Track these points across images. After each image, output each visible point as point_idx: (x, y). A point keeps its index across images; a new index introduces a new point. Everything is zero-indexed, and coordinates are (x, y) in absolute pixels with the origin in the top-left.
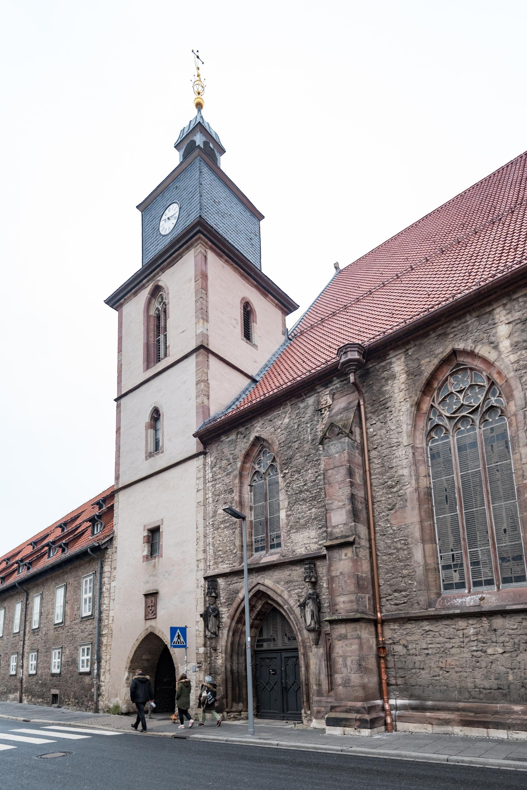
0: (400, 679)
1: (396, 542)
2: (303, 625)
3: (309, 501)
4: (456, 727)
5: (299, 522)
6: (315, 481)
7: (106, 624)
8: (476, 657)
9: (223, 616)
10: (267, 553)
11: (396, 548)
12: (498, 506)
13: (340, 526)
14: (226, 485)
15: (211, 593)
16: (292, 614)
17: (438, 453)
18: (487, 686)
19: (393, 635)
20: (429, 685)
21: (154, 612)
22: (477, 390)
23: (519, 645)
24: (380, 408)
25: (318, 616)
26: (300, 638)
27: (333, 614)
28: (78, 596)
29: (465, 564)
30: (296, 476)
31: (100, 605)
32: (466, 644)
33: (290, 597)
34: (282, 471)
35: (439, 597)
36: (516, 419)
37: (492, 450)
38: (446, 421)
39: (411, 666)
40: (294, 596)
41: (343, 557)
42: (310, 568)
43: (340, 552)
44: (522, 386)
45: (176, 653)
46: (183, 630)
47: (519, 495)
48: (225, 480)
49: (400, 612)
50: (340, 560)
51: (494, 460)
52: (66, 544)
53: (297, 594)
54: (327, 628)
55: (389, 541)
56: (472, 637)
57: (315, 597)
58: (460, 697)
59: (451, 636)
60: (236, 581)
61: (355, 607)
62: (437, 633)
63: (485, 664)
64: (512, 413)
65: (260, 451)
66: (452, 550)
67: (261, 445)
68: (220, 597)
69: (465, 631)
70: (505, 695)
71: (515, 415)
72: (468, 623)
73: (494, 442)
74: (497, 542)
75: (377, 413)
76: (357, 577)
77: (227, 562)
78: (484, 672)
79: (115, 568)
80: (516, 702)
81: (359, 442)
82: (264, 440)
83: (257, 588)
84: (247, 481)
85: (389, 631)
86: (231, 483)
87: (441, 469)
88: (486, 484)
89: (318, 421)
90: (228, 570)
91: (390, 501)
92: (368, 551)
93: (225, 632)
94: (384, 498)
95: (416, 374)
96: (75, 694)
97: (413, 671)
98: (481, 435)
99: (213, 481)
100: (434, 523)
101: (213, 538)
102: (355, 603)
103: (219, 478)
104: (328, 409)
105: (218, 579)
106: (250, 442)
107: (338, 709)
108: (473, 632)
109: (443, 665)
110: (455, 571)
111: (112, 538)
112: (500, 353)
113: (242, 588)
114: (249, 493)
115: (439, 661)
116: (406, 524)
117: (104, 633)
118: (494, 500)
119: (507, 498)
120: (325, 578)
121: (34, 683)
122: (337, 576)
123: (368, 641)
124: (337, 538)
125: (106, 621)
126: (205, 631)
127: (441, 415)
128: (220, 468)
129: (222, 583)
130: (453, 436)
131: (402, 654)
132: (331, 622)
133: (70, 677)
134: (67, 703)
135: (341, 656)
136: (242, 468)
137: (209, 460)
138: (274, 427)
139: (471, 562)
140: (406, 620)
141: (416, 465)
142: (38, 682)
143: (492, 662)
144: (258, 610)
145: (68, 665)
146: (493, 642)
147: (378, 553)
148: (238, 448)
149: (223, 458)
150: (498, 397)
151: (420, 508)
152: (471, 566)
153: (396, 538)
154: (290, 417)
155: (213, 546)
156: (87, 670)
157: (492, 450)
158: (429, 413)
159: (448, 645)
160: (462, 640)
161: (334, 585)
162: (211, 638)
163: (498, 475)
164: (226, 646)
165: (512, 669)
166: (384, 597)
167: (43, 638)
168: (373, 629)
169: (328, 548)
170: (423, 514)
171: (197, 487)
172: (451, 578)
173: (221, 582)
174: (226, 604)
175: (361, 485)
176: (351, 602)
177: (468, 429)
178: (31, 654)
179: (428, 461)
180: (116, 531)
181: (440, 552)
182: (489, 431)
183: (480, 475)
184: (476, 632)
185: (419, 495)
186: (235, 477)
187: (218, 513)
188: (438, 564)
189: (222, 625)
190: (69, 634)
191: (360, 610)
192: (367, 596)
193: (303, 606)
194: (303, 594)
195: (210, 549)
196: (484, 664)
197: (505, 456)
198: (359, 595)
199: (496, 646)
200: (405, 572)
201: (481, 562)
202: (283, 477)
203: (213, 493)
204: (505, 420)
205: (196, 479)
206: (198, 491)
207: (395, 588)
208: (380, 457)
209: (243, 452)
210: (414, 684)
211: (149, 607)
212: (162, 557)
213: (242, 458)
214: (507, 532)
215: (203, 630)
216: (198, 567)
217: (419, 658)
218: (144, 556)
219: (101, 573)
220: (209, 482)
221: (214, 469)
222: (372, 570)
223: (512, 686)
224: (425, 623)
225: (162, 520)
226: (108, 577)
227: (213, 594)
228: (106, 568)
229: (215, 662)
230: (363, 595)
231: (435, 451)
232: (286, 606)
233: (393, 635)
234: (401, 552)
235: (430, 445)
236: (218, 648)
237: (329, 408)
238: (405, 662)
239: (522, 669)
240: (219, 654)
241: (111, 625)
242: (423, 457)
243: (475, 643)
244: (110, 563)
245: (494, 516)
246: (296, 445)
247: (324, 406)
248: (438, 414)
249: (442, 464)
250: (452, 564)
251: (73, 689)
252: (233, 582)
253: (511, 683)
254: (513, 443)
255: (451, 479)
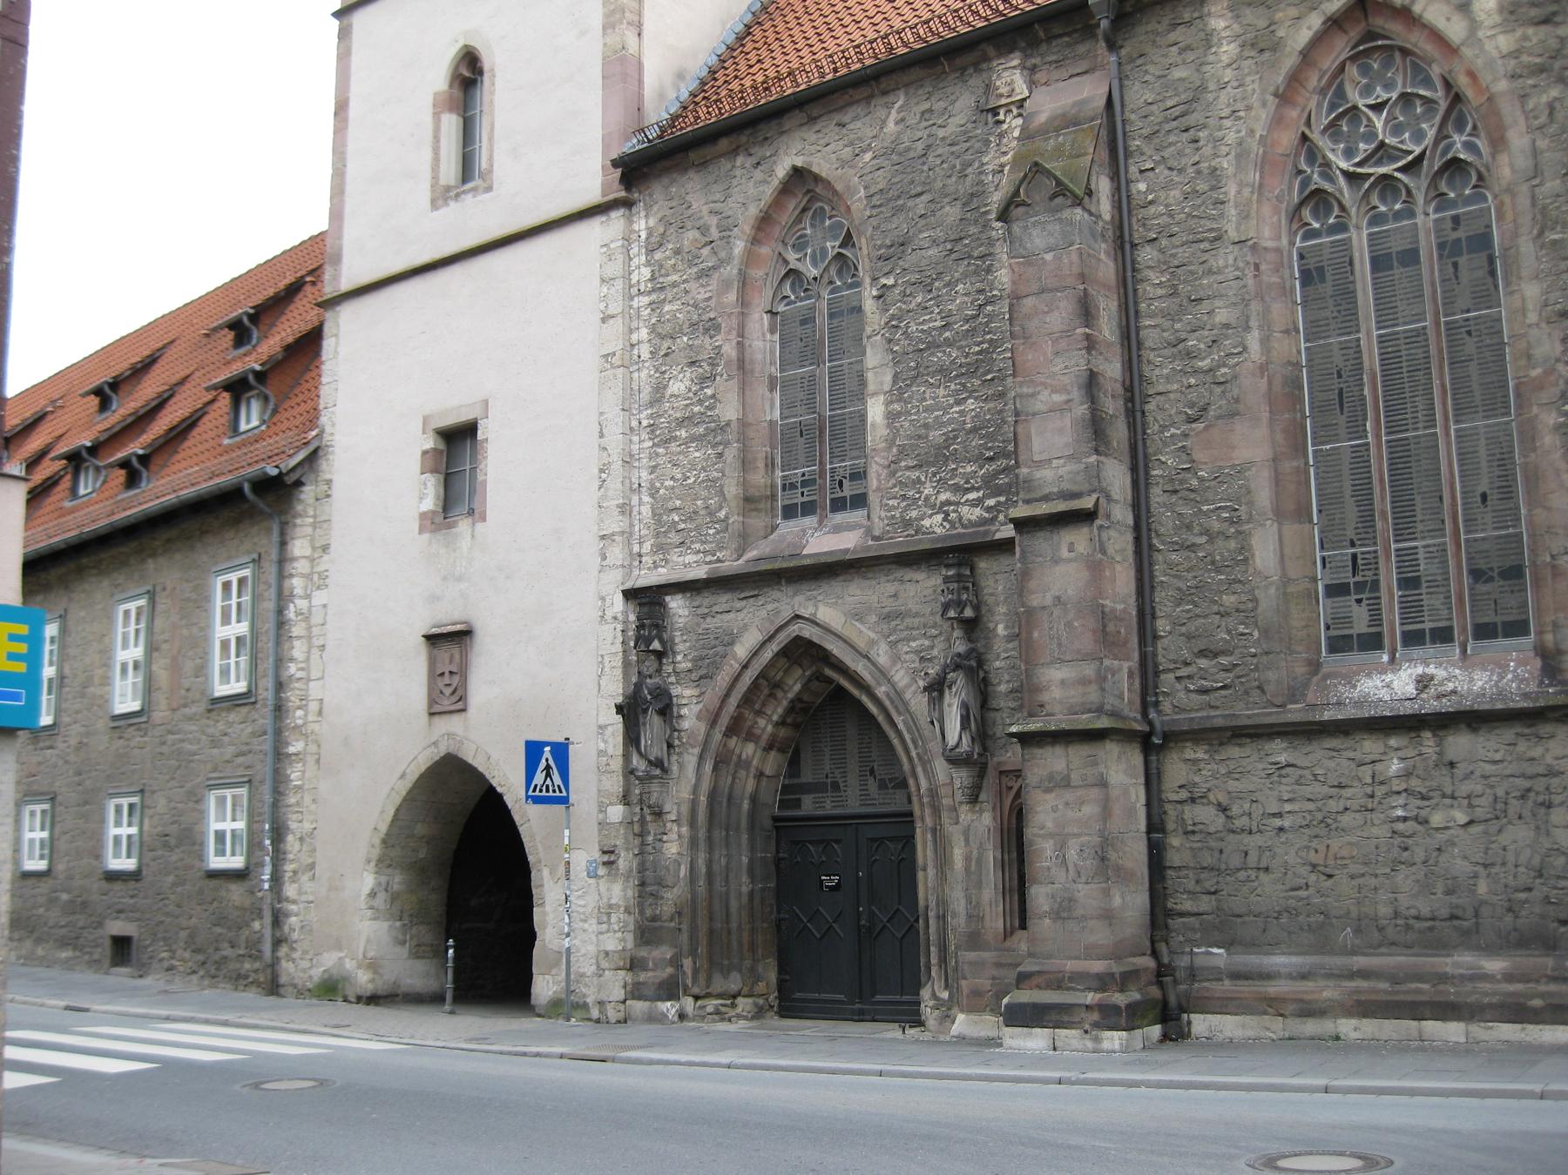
0: (1206, 898)
1: (1206, 514)
2: (935, 747)
3: (957, 376)
4: (1344, 1021)
5: (927, 437)
6: (975, 317)
7: (300, 722)
8: (1402, 835)
9: (685, 711)
10: (820, 522)
11: (1206, 532)
12: (1470, 428)
13: (1055, 463)
14: (696, 306)
15: (649, 641)
16: (899, 713)
17: (1321, 270)
18: (1425, 911)
19: (1191, 776)
20: (1279, 913)
21: (459, 693)
22: (1419, 110)
23: (1506, 803)
24: (1167, 127)
25: (979, 718)
26: (924, 784)
27: (1031, 715)
28: (195, 630)
29: (1383, 584)
30: (919, 299)
31: (280, 662)
32: (1380, 803)
33: (894, 663)
34: (875, 279)
35: (1316, 672)
36: (1514, 205)
37: (1457, 278)
38: (1342, 181)
39: (1236, 861)
40: (907, 657)
41: (1065, 553)
42: (959, 578)
43: (1055, 537)
44: (1527, 119)
45: (531, 821)
46: (561, 751)
47: (1519, 407)
48: (694, 293)
49: (1213, 713)
50: (1056, 561)
51: (1462, 303)
52: (144, 460)
53: (917, 652)
54: (1011, 755)
55: (1187, 511)
56: (1395, 781)
57: (973, 663)
58: (1357, 942)
59: (1343, 781)
60: (725, 607)
61: (1093, 696)
62: (1306, 772)
63: (1423, 854)
64: (1504, 183)
65: (804, 210)
66: (1353, 544)
67: (809, 191)
68: (674, 653)
69: (1379, 767)
70: (1466, 933)
71: (1509, 190)
72: (1386, 746)
73: (1460, 254)
74: (1465, 526)
75: (1157, 141)
76: (1103, 613)
77: (697, 546)
78: (1421, 876)
79: (325, 548)
80: (1490, 950)
81: (1107, 217)
82: (817, 178)
83: (795, 629)
84: (762, 300)
85: (1182, 765)
86: (712, 303)
87: (1328, 314)
88: (1441, 367)
89: (987, 142)
90: (700, 573)
91: (1193, 396)
92: (1129, 537)
93: (691, 760)
94: (1175, 387)
95: (1262, 45)
96: (192, 936)
97: (1242, 875)
98: (1428, 232)
99: (653, 290)
100: (1307, 463)
101: (653, 469)
102: (1093, 688)
103: (674, 285)
104: (1015, 111)
105: (668, 598)
106: (775, 183)
107: (1035, 980)
108: (1399, 770)
109: (1317, 859)
110: (1359, 601)
111: (315, 451)
112: (1474, 25)
113: (745, 627)
114: (768, 336)
115: (1308, 848)
116: (1233, 467)
117: (291, 750)
118: (1460, 412)
119: (1490, 412)
120: (1002, 609)
121: (41, 900)
122: (1044, 608)
123: (1126, 792)
124: (1046, 498)
125: (299, 713)
126: (626, 757)
127: (1327, 164)
128: (677, 252)
129: (681, 612)
130: (1358, 227)
131: (1212, 829)
132: (1026, 739)
133: (174, 885)
134: (166, 964)
135: (1051, 835)
136: (750, 258)
137: (641, 225)
138: (851, 144)
139: (1398, 579)
140: (1229, 734)
141: (1262, 299)
142: (57, 899)
143: (1439, 849)
144: (790, 695)
145: (166, 845)
146: (1444, 796)
147: (1155, 541)
148: (737, 197)
149: (689, 224)
150: (1469, 135)
151: (1271, 421)
152: (1400, 588)
153: (1207, 502)
154: (903, 120)
155: (652, 496)
156: (236, 862)
157: (1457, 278)
158: (1297, 155)
159: (1333, 805)
160: (1369, 790)
161: (1036, 635)
162: (647, 779)
163: (1470, 346)
164: (694, 803)
165: (1485, 866)
166: (1170, 670)
167: (72, 758)
168: (1137, 759)
169: (1021, 524)
170: (1279, 437)
171: (602, 306)
172: (1347, 620)
173: (677, 605)
174: (694, 676)
175: (1113, 343)
176: (1084, 682)
177: (1398, 212)
178: (29, 808)
179: (1293, 288)
180: (328, 429)
181: (1322, 548)
182: (1449, 224)
183: (1427, 340)
184: (1406, 769)
185: (1270, 383)
186: (726, 285)
187: (669, 392)
188: (1315, 580)
189: (679, 738)
190: (165, 749)
191: (1107, 707)
192: (1126, 665)
193: (936, 688)
194: (935, 652)
195: (641, 503)
196: (1420, 854)
197: (1486, 296)
198: (1107, 662)
199: (1452, 806)
200: (1229, 600)
201: (1424, 579)
202: (879, 297)
203: (653, 330)
204: (1485, 199)
205: (598, 282)
206: (604, 320)
207: (1201, 644)
208: (1164, 266)
209: (754, 211)
210: (1243, 910)
211: (442, 674)
212: (484, 519)
213: (747, 229)
214: (1489, 503)
215: (620, 751)
216: (604, 558)
217: (1258, 840)
218: (423, 516)
219: (283, 560)
220: (640, 293)
221: (658, 256)
222: (1140, 592)
223: (1485, 911)
224: (1278, 744)
225: (486, 403)
226: (303, 576)
227: (656, 645)
228: (299, 547)
229: (658, 851)
230: (1116, 662)
231: (1312, 263)
232: (883, 689)
233: (1191, 776)
234: (1220, 543)
235: (1298, 244)
236: (667, 808)
237: (1018, 108)
238: (1221, 852)
239: (1510, 866)
240: (669, 825)
241: (316, 727)
242: (1282, 278)
243: (1401, 800)
244: (309, 530)
245: (1459, 454)
246: (920, 205)
247: (1003, 101)
248: (1320, 161)
249: (1331, 302)
250: (1352, 581)
251: (185, 923)
252: (716, 609)
253: (1483, 903)
254: (1505, 265)
255: (1354, 344)
